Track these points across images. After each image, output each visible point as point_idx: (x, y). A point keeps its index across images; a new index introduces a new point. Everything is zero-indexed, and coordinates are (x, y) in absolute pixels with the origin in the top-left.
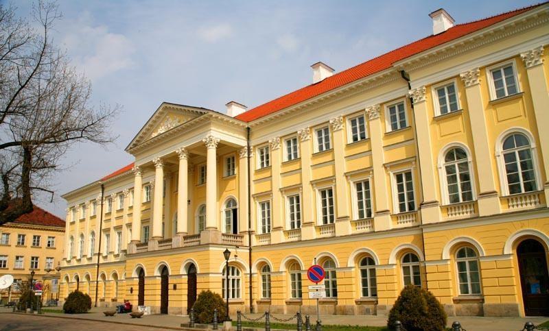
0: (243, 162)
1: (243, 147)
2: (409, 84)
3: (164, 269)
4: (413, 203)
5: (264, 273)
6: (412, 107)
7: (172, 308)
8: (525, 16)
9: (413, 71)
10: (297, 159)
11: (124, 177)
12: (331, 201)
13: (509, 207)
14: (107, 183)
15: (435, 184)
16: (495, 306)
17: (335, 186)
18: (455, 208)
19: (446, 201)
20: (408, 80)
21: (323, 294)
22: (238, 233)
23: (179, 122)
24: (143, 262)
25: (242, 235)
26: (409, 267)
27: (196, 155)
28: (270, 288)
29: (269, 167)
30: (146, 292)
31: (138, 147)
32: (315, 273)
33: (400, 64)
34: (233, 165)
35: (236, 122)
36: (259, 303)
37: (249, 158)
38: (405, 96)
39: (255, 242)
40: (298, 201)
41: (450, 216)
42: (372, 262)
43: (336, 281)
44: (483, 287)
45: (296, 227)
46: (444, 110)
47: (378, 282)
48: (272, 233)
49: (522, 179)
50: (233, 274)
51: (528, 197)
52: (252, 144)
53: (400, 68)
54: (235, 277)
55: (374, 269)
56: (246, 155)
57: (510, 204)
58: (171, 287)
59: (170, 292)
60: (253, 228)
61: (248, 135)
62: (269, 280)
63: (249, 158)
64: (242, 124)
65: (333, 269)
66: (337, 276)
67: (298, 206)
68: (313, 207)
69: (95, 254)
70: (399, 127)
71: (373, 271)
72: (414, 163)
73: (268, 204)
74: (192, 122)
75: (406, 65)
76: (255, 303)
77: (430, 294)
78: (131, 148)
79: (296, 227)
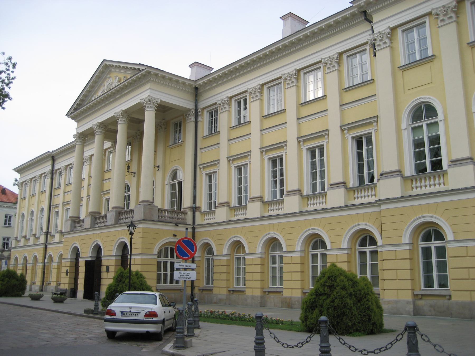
0: (190, 128)
1: (190, 110)
4: (324, 170)
7: (389, 302)
16: (464, 305)
17: (376, 131)
20: (370, 22)
22: (182, 209)
25: (185, 210)
26: (365, 252)
28: (244, 273)
31: (78, 111)
34: (180, 130)
37: (196, 122)
42: (439, 236)
44: (61, 278)
45: (319, 190)
48: (249, 205)
49: (429, 159)
51: (432, 178)
53: (362, 7)
55: (444, 247)
56: (193, 119)
57: (414, 185)
60: (198, 204)
61: (196, 96)
63: (196, 122)
65: (323, 251)
67: (322, 162)
68: (296, 172)
71: (441, 252)
73: (281, 160)
76: (196, 291)
77: (145, 282)
78: (72, 113)
79: (319, 190)
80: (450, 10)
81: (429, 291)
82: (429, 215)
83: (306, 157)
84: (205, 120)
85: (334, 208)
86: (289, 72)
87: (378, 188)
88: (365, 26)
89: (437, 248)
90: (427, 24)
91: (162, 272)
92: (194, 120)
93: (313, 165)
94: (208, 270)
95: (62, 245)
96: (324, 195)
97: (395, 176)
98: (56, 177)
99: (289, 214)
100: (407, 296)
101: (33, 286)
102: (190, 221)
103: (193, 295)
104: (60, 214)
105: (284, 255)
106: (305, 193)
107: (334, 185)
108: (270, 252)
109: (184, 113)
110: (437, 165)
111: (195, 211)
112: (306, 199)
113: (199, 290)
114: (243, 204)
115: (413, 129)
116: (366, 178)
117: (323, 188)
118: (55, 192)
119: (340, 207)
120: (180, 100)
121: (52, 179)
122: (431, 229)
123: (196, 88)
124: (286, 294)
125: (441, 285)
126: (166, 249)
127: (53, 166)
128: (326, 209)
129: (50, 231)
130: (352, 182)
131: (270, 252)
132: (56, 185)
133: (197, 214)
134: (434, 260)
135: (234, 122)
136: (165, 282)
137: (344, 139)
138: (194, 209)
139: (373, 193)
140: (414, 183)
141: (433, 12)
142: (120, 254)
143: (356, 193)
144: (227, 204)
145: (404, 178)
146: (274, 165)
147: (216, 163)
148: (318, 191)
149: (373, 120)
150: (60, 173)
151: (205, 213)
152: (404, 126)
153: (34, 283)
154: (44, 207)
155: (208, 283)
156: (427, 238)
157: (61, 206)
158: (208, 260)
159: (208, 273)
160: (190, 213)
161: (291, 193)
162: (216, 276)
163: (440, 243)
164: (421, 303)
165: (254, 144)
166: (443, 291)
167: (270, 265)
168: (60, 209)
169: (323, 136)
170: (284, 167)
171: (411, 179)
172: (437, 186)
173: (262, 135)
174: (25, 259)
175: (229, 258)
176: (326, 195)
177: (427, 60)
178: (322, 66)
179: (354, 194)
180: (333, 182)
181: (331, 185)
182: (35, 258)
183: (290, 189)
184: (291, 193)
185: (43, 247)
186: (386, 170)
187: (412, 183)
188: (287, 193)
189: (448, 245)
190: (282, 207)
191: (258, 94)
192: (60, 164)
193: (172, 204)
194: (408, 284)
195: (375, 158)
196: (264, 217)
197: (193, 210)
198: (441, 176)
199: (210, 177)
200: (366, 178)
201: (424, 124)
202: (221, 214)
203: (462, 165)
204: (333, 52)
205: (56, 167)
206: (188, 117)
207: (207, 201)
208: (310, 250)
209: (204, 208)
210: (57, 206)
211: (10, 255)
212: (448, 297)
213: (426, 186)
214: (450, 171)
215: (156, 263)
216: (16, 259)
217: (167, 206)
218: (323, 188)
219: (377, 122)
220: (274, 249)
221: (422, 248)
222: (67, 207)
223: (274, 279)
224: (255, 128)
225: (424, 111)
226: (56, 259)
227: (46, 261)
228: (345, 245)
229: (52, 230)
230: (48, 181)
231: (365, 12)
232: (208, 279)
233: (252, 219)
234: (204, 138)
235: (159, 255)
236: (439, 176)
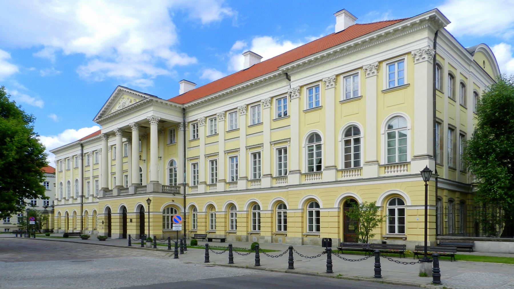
1: (180, 123)
3: (124, 209)
10: (216, 134)
11: (93, 140)
13: (385, 172)
14: (86, 142)
19: (341, 165)
20: (290, 80)
23: (131, 102)
24: (109, 202)
28: (259, 223)
30: (112, 224)
33: (284, 68)
35: (169, 103)
37: (185, 131)
39: (189, 191)
41: (387, 173)
47: (321, 221)
48: (199, 186)
50: (172, 213)
56: (182, 129)
58: (128, 220)
59: (128, 224)
60: (187, 183)
62: (285, 216)
63: (185, 131)
64: (178, 105)
67: (286, 157)
73: (216, 162)
75: (288, 69)
76: (187, 233)
78: (97, 119)
80: (424, 52)
81: (392, 235)
83: (275, 154)
87: (323, 174)
88: (285, 83)
89: (399, 210)
90: (406, 61)
91: (166, 222)
93: (280, 159)
94: (194, 220)
96: (259, 180)
97: (296, 173)
98: (86, 158)
100: (300, 235)
101: (94, 231)
102: (182, 192)
103: (185, 235)
104: (91, 184)
105: (261, 212)
110: (357, 164)
115: (309, 147)
116: (283, 173)
118: (85, 169)
121: (82, 160)
124: (238, 234)
125: (399, 232)
126: (168, 209)
127: (82, 150)
128: (261, 188)
130: (275, 174)
132: (86, 164)
134: (396, 216)
135: (275, 116)
136: (168, 227)
138: (185, 185)
139: (359, 173)
141: (323, 80)
142: (122, 212)
144: (205, 183)
145: (380, 166)
146: (213, 165)
148: (283, 174)
149: (288, 140)
150: (88, 155)
151: (192, 187)
152: (340, 138)
155: (194, 228)
156: (311, 206)
157: (91, 178)
158: (194, 215)
159: (194, 222)
160: (182, 188)
161: (242, 178)
162: (199, 224)
163: (401, 207)
164: (305, 239)
166: (401, 235)
168: (91, 180)
169: (197, 159)
170: (261, 159)
172: (399, 172)
173: (225, 143)
174: (67, 213)
177: (403, 86)
180: (327, 165)
182: (75, 212)
183: (241, 176)
184: (242, 178)
186: (292, 170)
187: (385, 169)
191: (223, 117)
192: (88, 149)
193: (171, 181)
194: (300, 230)
195: (288, 162)
199: (194, 165)
201: (314, 145)
202: (201, 189)
203: (330, 169)
205: (85, 152)
207: (193, 180)
209: (191, 184)
210: (88, 178)
211: (53, 210)
213: (391, 172)
214: (324, 172)
215: (162, 217)
216: (59, 213)
217: (167, 183)
218: (286, 174)
220: (232, 209)
221: (389, 209)
222: (114, 176)
223: (232, 226)
225: (315, 137)
226: (91, 213)
227: (83, 215)
229: (86, 194)
230: (80, 161)
231: (287, 74)
232: (194, 225)
234: (191, 141)
235: (164, 213)
236: (358, 170)
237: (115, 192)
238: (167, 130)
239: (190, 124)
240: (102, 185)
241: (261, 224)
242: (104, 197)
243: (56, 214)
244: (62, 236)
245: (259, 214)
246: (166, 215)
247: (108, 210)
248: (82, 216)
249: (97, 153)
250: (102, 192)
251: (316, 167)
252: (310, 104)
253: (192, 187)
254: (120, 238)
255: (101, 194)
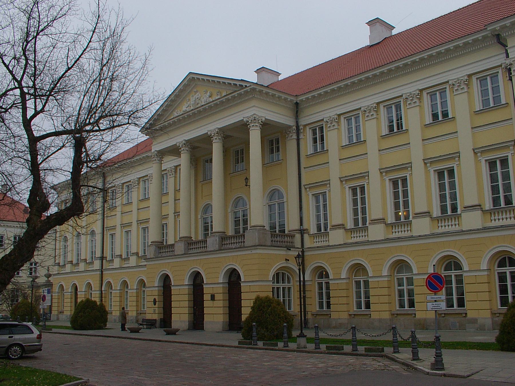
0: (291, 145)
1: (290, 127)
2: (507, 51)
5: (320, 280)
6: (511, 79)
8: (394, 66)
9: (511, 35)
10: (361, 142)
12: (363, 200)
15: (423, 192)
17: (368, 184)
18: (445, 220)
20: (505, 46)
21: (443, 306)
23: (210, 97)
24: (166, 266)
25: (292, 233)
27: (198, 147)
28: (328, 297)
29: (324, 151)
32: (434, 282)
33: (497, 26)
36: (315, 315)
37: (298, 140)
38: (501, 66)
39: (308, 243)
40: (325, 200)
42: (458, 266)
43: (413, 290)
46: (486, 102)
52: (303, 122)
54: (286, 285)
56: (295, 136)
60: (305, 226)
61: (297, 112)
62: (328, 288)
63: (298, 140)
64: (290, 98)
65: (409, 275)
66: (415, 283)
67: (325, 206)
69: (97, 258)
70: (395, 130)
72: (409, 169)
74: (235, 94)
75: (504, 27)
76: (309, 316)
82: (505, 245)
83: (348, 194)
84: (308, 137)
85: (470, 230)
86: (458, 77)
88: (498, 50)
92: (296, 137)
95: (146, 269)
97: (340, 228)
99: (420, 236)
101: (60, 316)
102: (298, 244)
106: (435, 215)
107: (468, 208)
108: (396, 275)
109: (284, 130)
110: (454, 209)
111: (304, 233)
112: (437, 221)
113: (313, 315)
114: (322, 231)
116: (361, 222)
117: (326, 229)
119: (478, 230)
120: (279, 115)
122: (506, 256)
123: (297, 104)
128: (329, 246)
129: (105, 256)
131: (396, 275)
133: (306, 236)
137: (427, 172)
138: (302, 232)
139: (457, 223)
140: (493, 216)
143: (394, 228)
145: (484, 212)
147: (114, 228)
151: (314, 236)
153: (62, 312)
154: (95, 229)
160: (298, 236)
163: (458, 272)
165: (373, 163)
166: (461, 310)
167: (397, 287)
169: (364, 177)
171: (490, 212)
173: (122, 216)
175: (348, 281)
176: (411, 224)
178: (360, 113)
179: (393, 229)
181: (371, 221)
185: (99, 273)
188: (331, 227)
189: (465, 274)
190: (366, 234)
196: (388, 239)
197: (301, 233)
198: (457, 218)
199: (112, 235)
200: (450, 209)
204: (462, 73)
206: (288, 134)
208: (316, 279)
210: (114, 228)
212: (413, 315)
218: (326, 229)
219: (459, 157)
224: (134, 207)
226: (117, 286)
227: (103, 289)
228: (385, 273)
229: (108, 254)
233: (375, 241)
237: (180, 248)
238: (274, 139)
239: (308, 128)
240: (153, 236)
241: (332, 301)
242: (156, 258)
243: (56, 288)
244: (491, 337)
245: (327, 283)
246: (276, 285)
247: (166, 280)
248: (102, 291)
249: (145, 181)
250: (153, 249)
251: (450, 209)
252: (350, 138)
253: (314, 236)
254: (189, 329)
255: (150, 253)
